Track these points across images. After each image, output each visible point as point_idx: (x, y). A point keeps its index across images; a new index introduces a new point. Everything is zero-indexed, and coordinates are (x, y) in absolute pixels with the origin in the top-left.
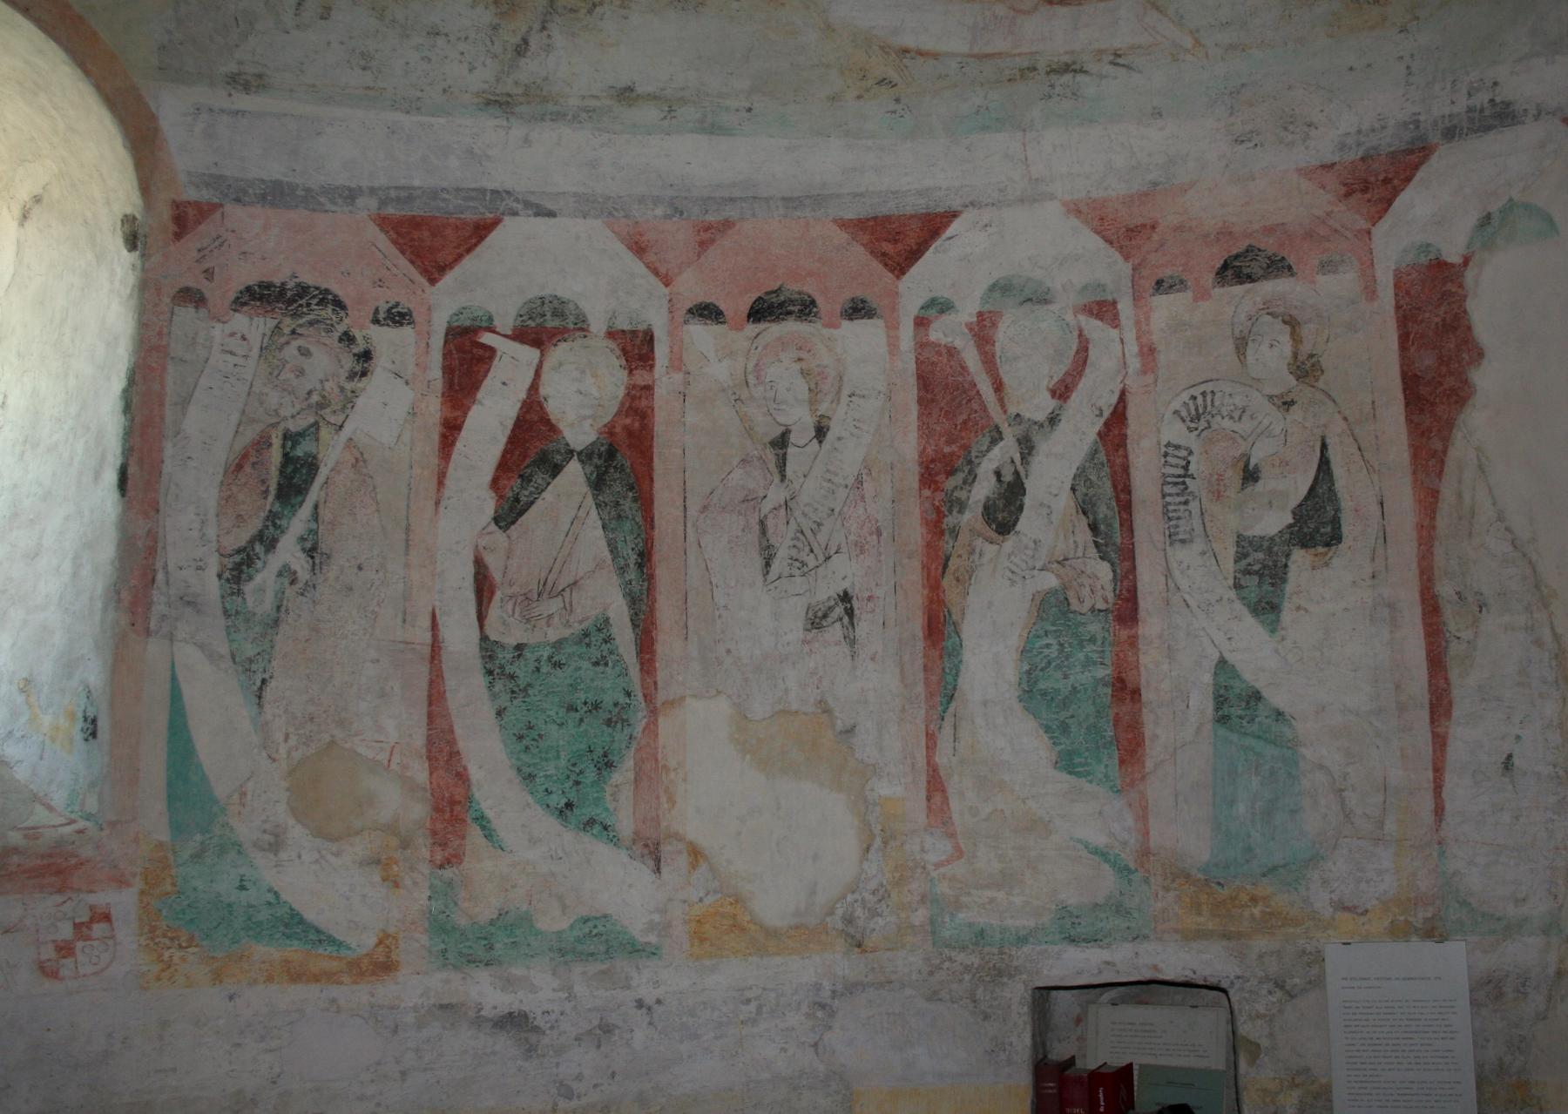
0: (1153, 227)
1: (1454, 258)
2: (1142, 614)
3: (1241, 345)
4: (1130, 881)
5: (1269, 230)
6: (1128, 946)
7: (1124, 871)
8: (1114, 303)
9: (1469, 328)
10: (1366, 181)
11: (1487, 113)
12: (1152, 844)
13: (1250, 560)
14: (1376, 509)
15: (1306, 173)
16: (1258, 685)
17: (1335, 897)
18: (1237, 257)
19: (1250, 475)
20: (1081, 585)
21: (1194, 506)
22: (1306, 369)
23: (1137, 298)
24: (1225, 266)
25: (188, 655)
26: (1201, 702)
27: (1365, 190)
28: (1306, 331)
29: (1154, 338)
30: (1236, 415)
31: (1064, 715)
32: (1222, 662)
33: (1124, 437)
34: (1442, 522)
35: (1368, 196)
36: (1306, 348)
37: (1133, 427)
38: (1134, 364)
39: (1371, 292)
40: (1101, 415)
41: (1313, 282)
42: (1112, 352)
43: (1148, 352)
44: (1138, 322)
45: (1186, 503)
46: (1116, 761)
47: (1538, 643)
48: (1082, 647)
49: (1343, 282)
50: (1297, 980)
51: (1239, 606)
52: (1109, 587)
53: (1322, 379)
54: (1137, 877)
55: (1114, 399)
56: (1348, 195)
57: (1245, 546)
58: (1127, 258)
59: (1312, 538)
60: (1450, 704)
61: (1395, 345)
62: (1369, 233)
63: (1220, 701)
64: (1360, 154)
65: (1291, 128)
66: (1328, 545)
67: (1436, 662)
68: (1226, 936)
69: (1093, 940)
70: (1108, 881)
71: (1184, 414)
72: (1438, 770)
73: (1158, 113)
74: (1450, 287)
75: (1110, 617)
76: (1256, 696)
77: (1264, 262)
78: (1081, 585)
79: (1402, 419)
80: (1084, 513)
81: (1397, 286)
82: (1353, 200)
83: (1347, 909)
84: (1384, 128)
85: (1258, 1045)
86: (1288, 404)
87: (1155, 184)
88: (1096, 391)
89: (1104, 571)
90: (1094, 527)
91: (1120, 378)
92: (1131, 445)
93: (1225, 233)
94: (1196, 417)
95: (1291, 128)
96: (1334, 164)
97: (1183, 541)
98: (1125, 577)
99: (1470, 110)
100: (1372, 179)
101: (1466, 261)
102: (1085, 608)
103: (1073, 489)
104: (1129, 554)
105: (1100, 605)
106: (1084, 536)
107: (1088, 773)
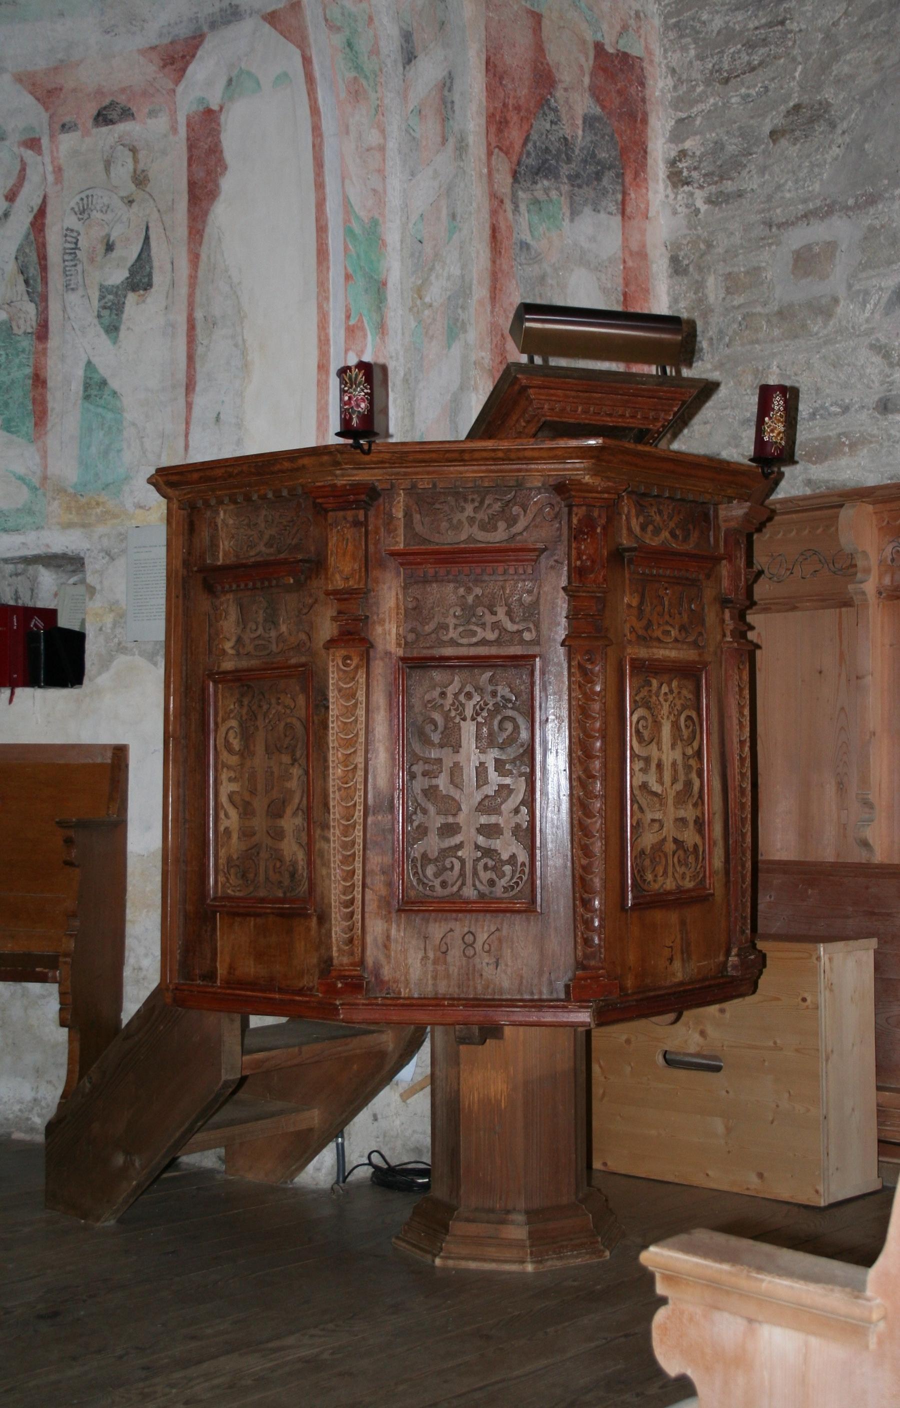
0: (61, 89)
1: (215, 108)
2: (51, 335)
3: (108, 165)
4: (36, 496)
5: (123, 90)
6: (33, 533)
7: (34, 489)
8: (39, 140)
9: (222, 151)
10: (173, 58)
11: (228, 12)
12: (49, 473)
13: (106, 300)
14: (170, 266)
15: (143, 52)
16: (105, 376)
17: (136, 500)
18: (105, 108)
19: (109, 247)
20: (20, 318)
21: (79, 268)
22: (140, 180)
23: (52, 136)
24: (99, 114)
25: (456, 678)
26: (77, 387)
27: (172, 64)
28: (141, 155)
29: (61, 161)
30: (104, 210)
31: (6, 397)
32: (89, 363)
33: (43, 225)
34: (200, 274)
35: (174, 67)
36: (141, 166)
37: (49, 219)
38: (51, 178)
39: (174, 130)
40: (32, 211)
41: (145, 123)
42: (39, 169)
43: (58, 171)
44: (52, 152)
45: (75, 265)
46: (33, 424)
47: (236, 345)
48: (18, 355)
49: (160, 124)
50: (116, 550)
51: (99, 327)
52: (34, 318)
53: (149, 186)
54: (40, 492)
55: (40, 201)
56: (164, 66)
57: (104, 291)
58: (47, 110)
59: (138, 286)
60: (195, 383)
61: (185, 164)
62: (174, 91)
63: (87, 386)
64: (170, 39)
65: (134, 22)
66: (145, 289)
67: (191, 358)
68: (83, 526)
69: (17, 530)
70: (24, 496)
71: (76, 209)
72: (188, 423)
73: (62, 15)
74: (213, 125)
75: (34, 337)
76: (104, 383)
77: (119, 111)
78: (20, 318)
79: (186, 209)
80: (22, 273)
81: (188, 125)
82: (166, 70)
83: (141, 507)
84: (181, 22)
85: (94, 588)
86: (131, 202)
87: (62, 61)
88: (29, 198)
89: (31, 309)
90: (26, 282)
91: (43, 187)
92: (47, 231)
93: (100, 92)
94: (83, 212)
95: (134, 22)
96: (157, 46)
97: (73, 289)
98: (43, 312)
99: (221, 10)
100: (176, 56)
101: (221, 108)
102: (21, 332)
103: (16, 258)
104: (44, 298)
105: (29, 330)
106: (22, 287)
107: (18, 431)
